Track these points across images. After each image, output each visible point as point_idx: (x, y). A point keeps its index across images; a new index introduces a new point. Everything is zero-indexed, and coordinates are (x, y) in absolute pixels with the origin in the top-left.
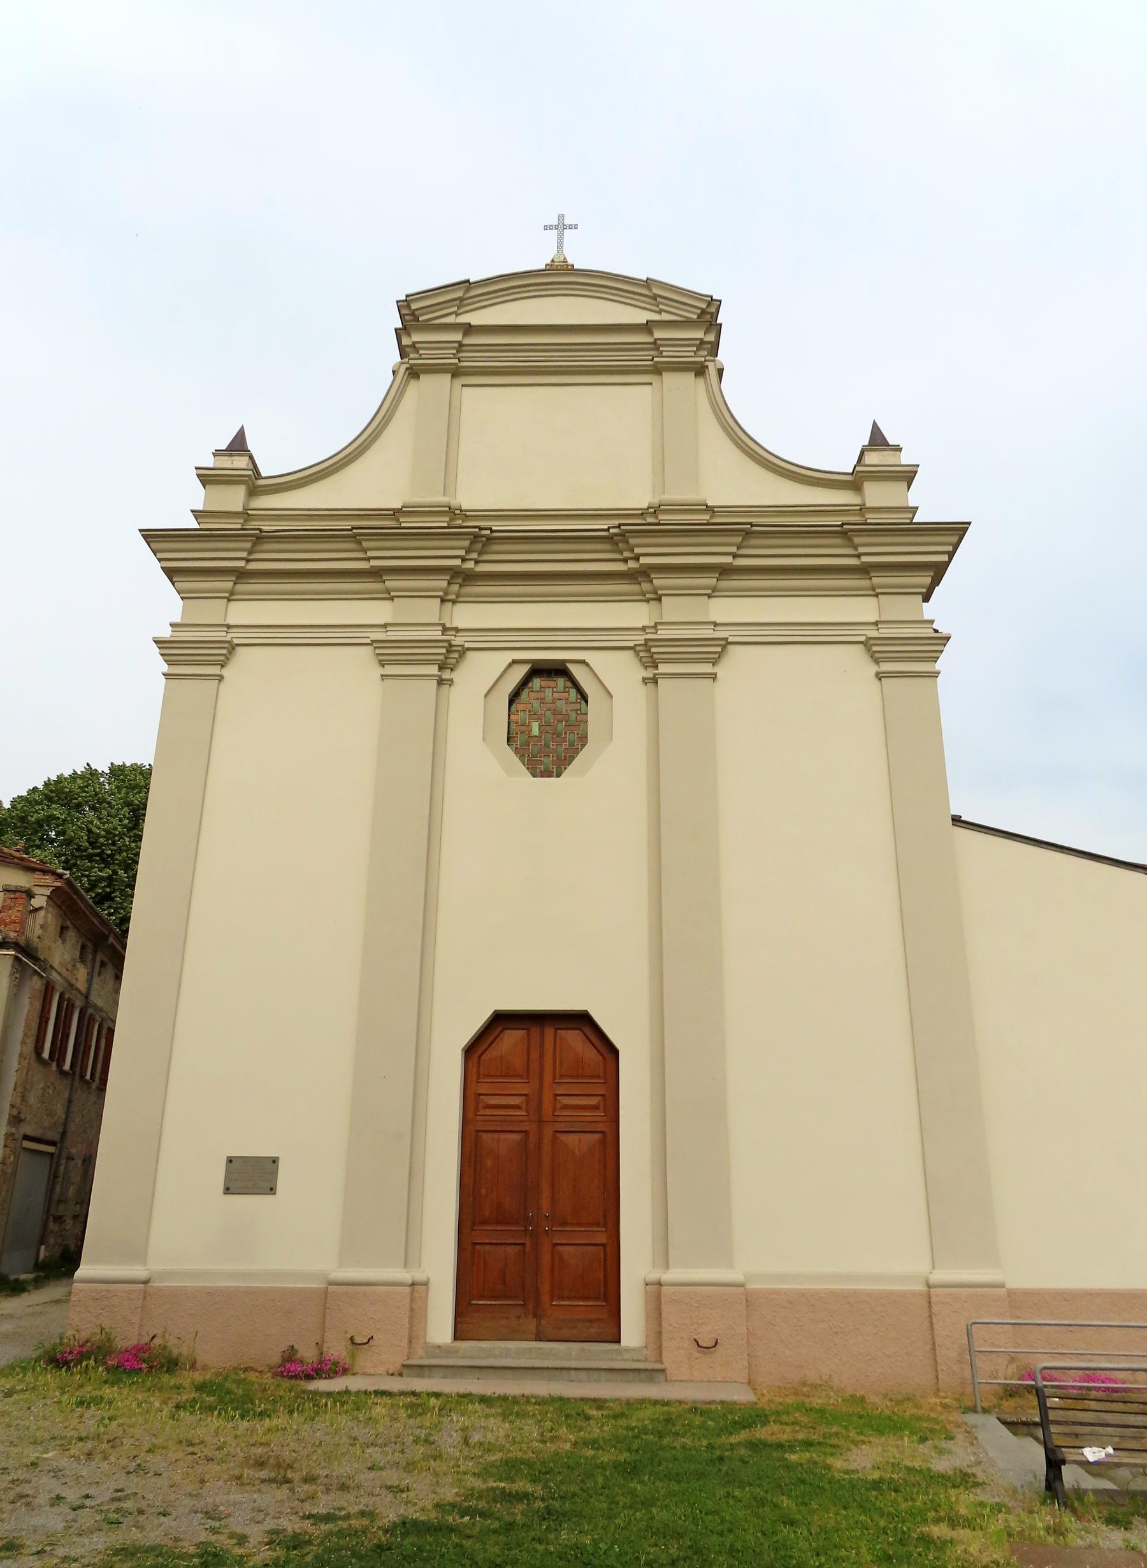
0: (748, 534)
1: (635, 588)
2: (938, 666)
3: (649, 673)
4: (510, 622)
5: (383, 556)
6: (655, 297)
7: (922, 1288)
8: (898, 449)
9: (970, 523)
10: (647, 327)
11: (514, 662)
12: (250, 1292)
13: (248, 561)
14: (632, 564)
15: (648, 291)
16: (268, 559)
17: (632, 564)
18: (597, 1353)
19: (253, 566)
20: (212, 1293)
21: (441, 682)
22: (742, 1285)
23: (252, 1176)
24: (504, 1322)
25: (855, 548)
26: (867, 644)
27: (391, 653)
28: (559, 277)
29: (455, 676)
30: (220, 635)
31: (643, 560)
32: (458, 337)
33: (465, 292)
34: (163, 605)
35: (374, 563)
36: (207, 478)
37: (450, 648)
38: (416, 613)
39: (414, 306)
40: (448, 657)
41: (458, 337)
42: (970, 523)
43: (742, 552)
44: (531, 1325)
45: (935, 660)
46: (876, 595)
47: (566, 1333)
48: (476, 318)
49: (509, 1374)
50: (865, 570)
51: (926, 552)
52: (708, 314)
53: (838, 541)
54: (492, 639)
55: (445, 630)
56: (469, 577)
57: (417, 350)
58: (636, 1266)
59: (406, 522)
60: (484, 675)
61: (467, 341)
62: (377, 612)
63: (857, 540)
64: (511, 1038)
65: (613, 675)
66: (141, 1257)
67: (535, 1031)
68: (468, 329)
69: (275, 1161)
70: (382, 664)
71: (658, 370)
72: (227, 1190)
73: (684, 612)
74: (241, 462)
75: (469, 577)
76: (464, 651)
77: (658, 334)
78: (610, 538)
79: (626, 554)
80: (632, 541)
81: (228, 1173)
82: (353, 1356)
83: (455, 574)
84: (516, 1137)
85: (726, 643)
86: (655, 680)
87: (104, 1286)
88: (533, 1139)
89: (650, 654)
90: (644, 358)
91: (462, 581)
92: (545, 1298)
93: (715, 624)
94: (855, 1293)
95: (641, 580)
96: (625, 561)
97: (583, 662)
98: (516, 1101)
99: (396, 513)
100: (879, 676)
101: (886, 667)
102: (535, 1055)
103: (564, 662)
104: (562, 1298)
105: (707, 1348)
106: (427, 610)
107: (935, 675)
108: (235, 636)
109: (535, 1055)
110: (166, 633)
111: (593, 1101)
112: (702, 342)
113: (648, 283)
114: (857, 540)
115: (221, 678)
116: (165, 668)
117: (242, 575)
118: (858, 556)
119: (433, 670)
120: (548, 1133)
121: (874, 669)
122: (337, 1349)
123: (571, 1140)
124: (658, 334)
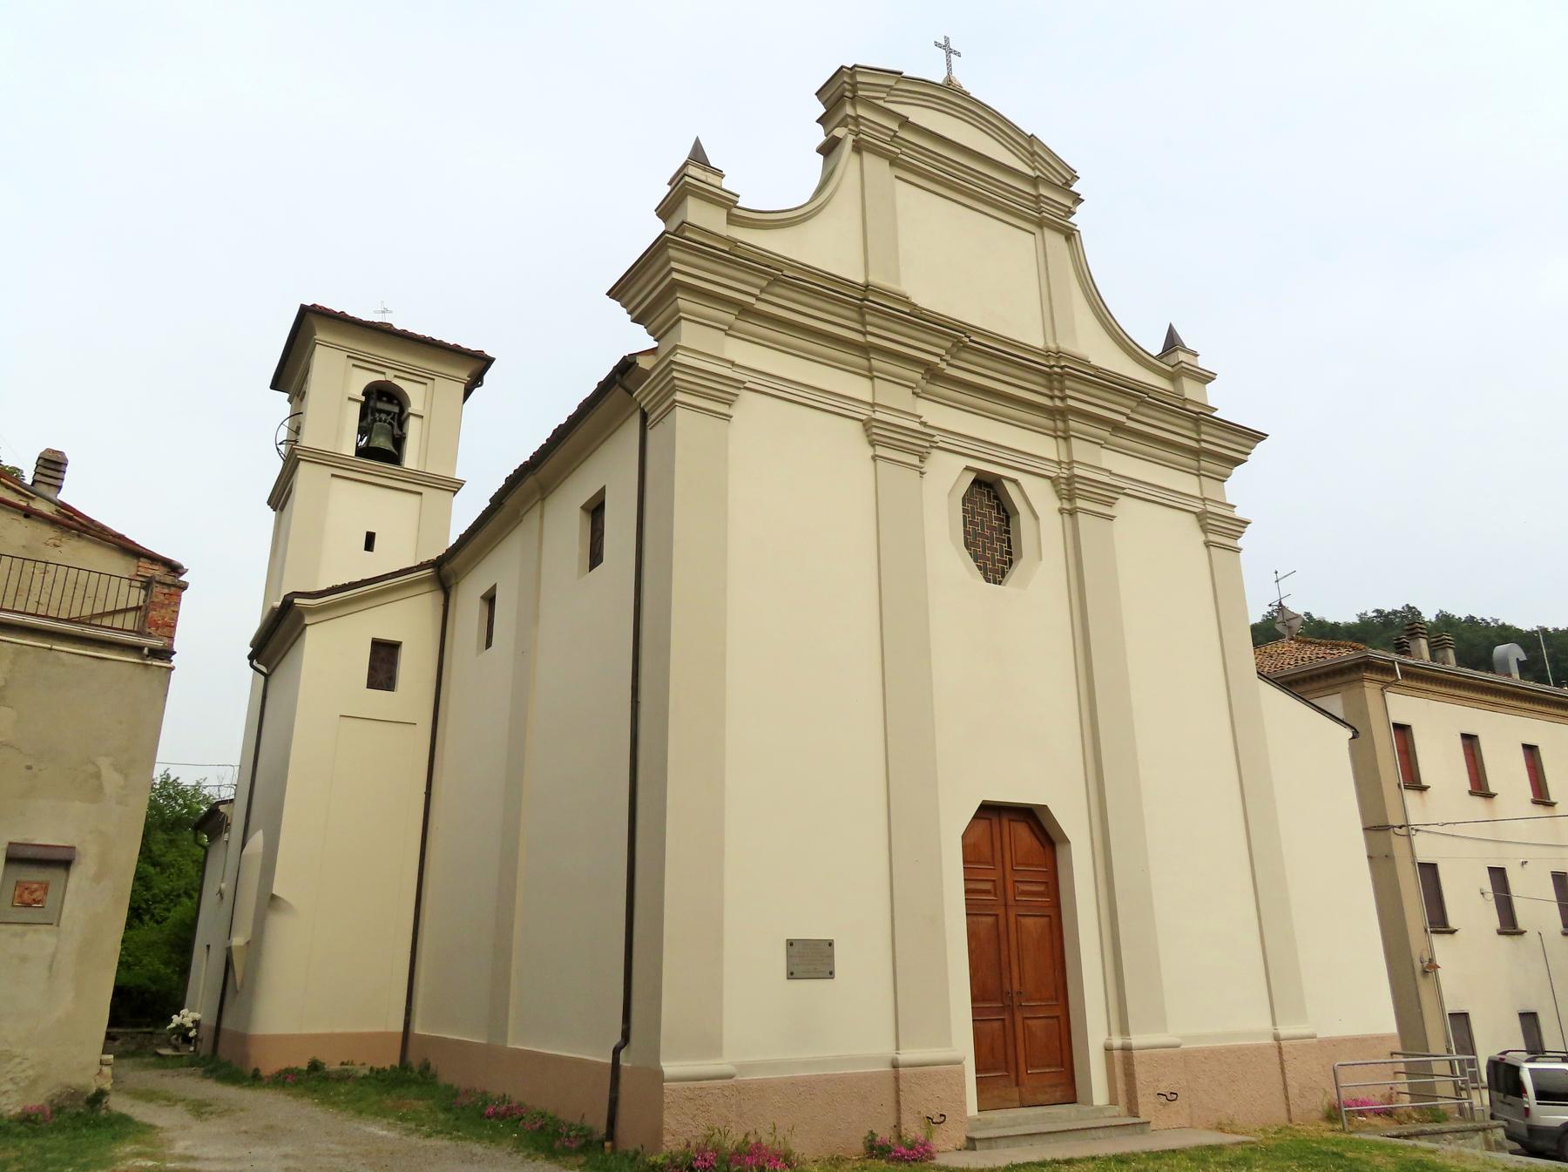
0: (776, 281)
1: (1050, 423)
2: (1240, 543)
3: (1067, 505)
6: (1033, 154)
7: (1270, 1041)
8: (719, 173)
9: (1259, 437)
12: (829, 1080)
14: (1058, 403)
15: (1030, 146)
17: (1058, 403)
18: (1062, 1115)
20: (794, 1083)
22: (731, 1077)
23: (810, 959)
24: (996, 1092)
25: (864, 324)
26: (867, 425)
27: (879, 434)
28: (950, 96)
31: (1070, 402)
32: (895, 127)
35: (870, 339)
38: (897, 399)
39: (860, 78)
42: (1259, 437)
43: (764, 296)
44: (1014, 1093)
45: (729, 404)
46: (871, 378)
47: (1041, 1098)
49: (1051, 1138)
50: (865, 350)
51: (1221, 445)
53: (1190, 425)
54: (959, 444)
57: (857, 124)
58: (1096, 1031)
60: (947, 477)
61: (900, 134)
63: (1204, 428)
64: (1022, 832)
66: (713, 1047)
68: (905, 122)
69: (790, 943)
71: (1041, 224)
72: (791, 975)
77: (1043, 191)
79: (1057, 393)
80: (1068, 383)
81: (789, 956)
82: (930, 1133)
84: (990, 920)
85: (1120, 491)
86: (1072, 513)
87: (691, 1084)
88: (1002, 921)
89: (1068, 488)
92: (1022, 1066)
93: (733, 364)
94: (1240, 1048)
95: (1058, 420)
96: (1052, 398)
97: (1015, 481)
98: (988, 886)
100: (1208, 544)
101: (1212, 537)
102: (997, 845)
103: (1000, 477)
104: (1033, 1067)
105: (1172, 1097)
107: (1237, 550)
109: (997, 845)
111: (1041, 888)
113: (1031, 139)
114: (1204, 428)
118: (864, 334)
121: (870, 452)
122: (913, 1130)
123: (1029, 922)
124: (1043, 191)
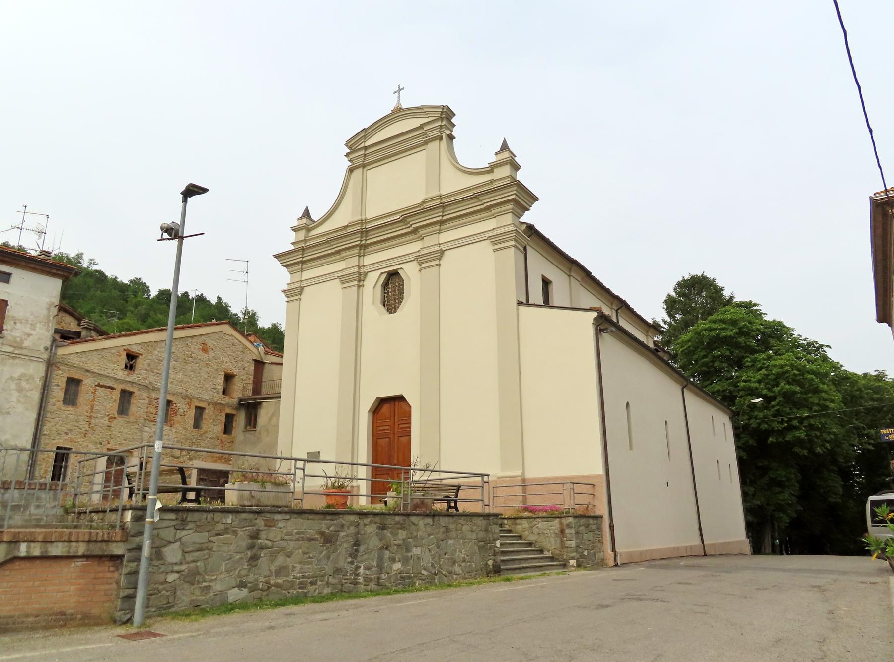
4: (379, 259)
5: (416, 223)
10: (421, 127)
11: (382, 273)
13: (443, 216)
16: (450, 213)
19: (445, 218)
21: (359, 286)
27: (344, 279)
28: (399, 113)
29: (365, 283)
30: (437, 248)
32: (363, 152)
33: (365, 133)
34: (283, 277)
36: (295, 230)
37: (360, 274)
40: (361, 277)
41: (363, 152)
48: (367, 144)
52: (447, 114)
55: (359, 267)
56: (366, 246)
59: (426, 206)
60: (374, 280)
62: (341, 265)
64: (386, 408)
65: (410, 272)
67: (393, 403)
68: (366, 148)
70: (342, 284)
73: (430, 242)
74: (506, 155)
75: (366, 246)
76: (366, 274)
78: (401, 221)
83: (360, 246)
89: (421, 259)
90: (420, 140)
91: (363, 248)
99: (345, 227)
106: (354, 261)
108: (443, 247)
110: (286, 287)
112: (441, 126)
113: (422, 107)
115: (439, 265)
116: (286, 299)
117: (441, 223)
119: (356, 283)
120: (396, 436)
